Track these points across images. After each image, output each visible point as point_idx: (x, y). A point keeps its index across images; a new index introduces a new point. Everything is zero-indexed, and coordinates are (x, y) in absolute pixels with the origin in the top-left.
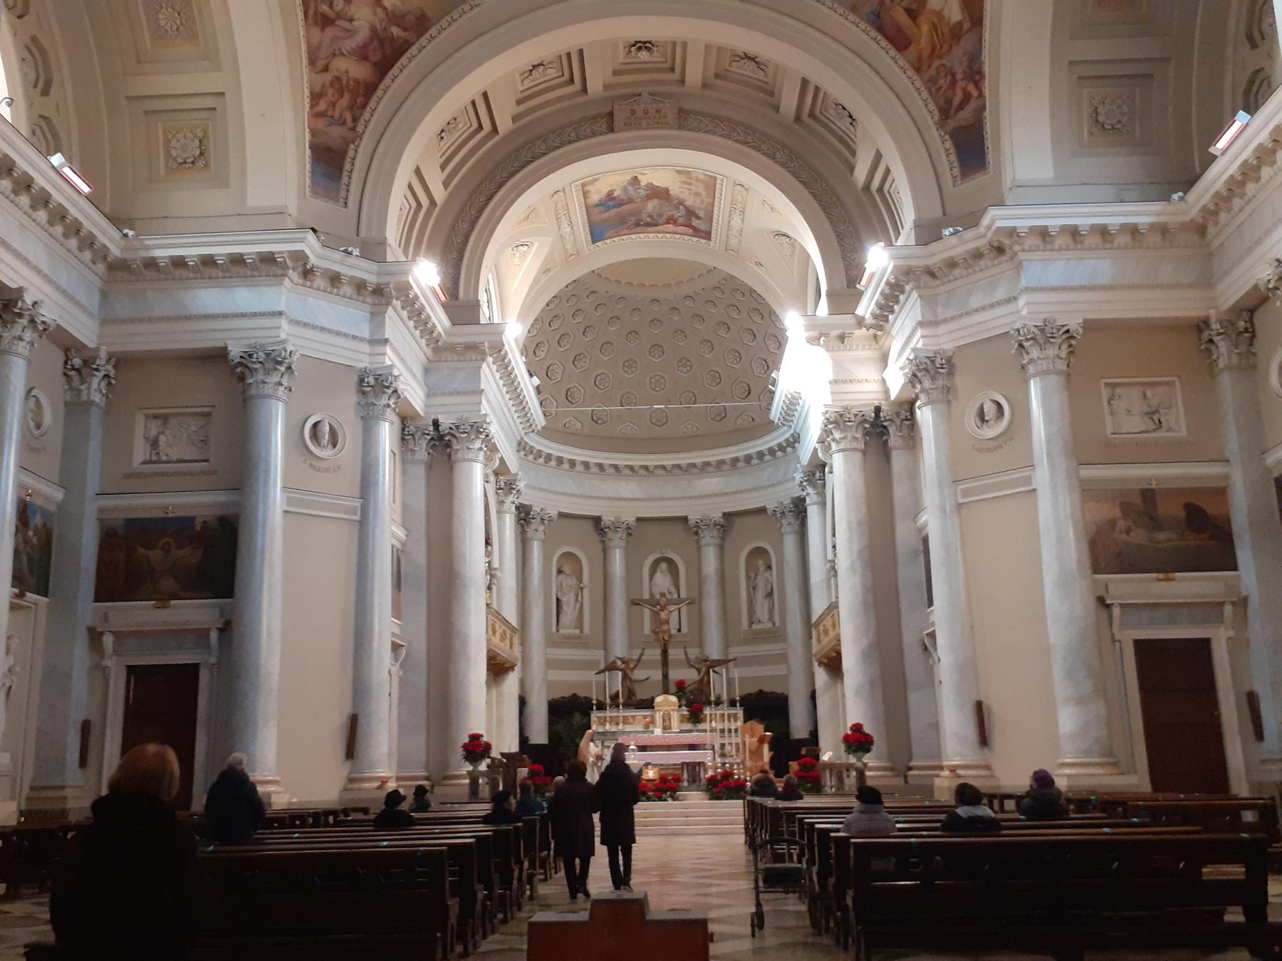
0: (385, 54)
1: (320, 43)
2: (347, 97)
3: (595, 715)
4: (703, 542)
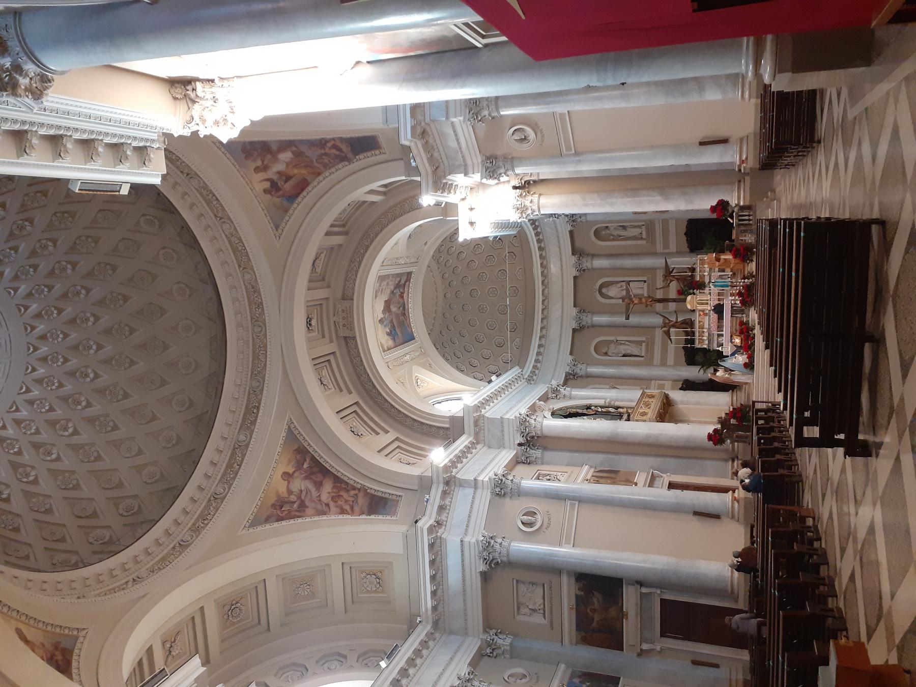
0: (318, 471)
2: (341, 493)
3: (697, 345)
4: (589, 266)
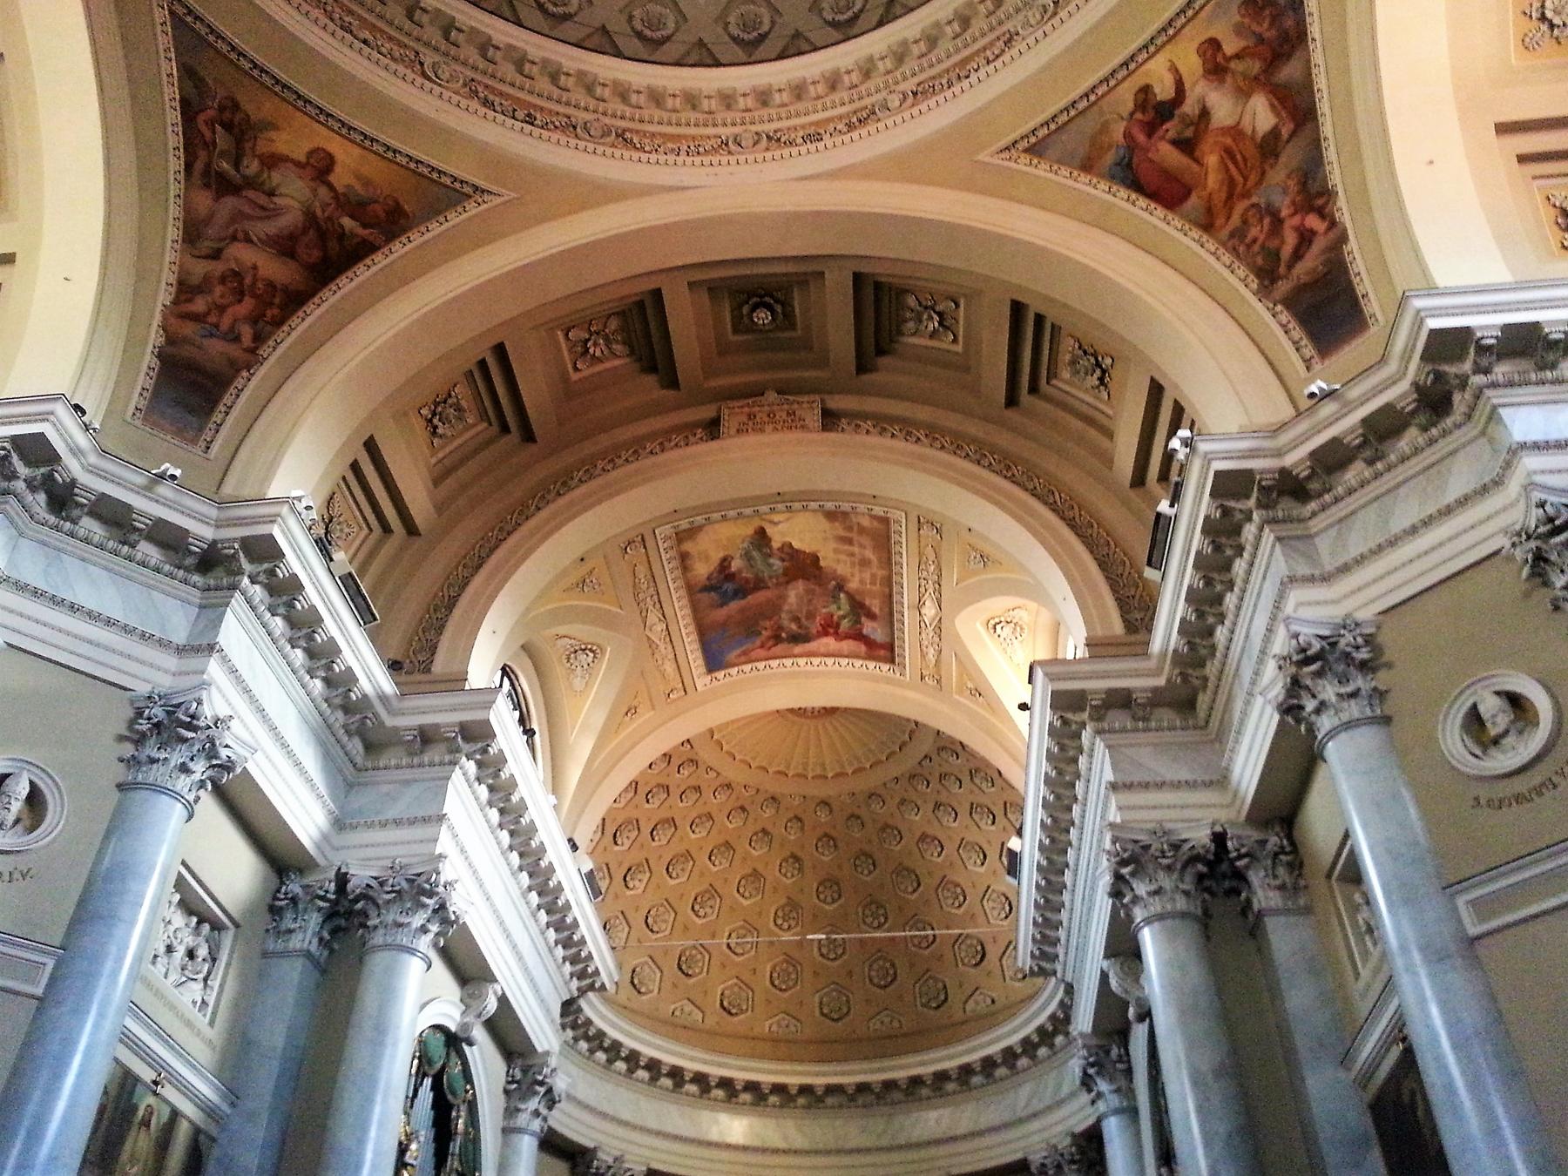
1: (211, 216)
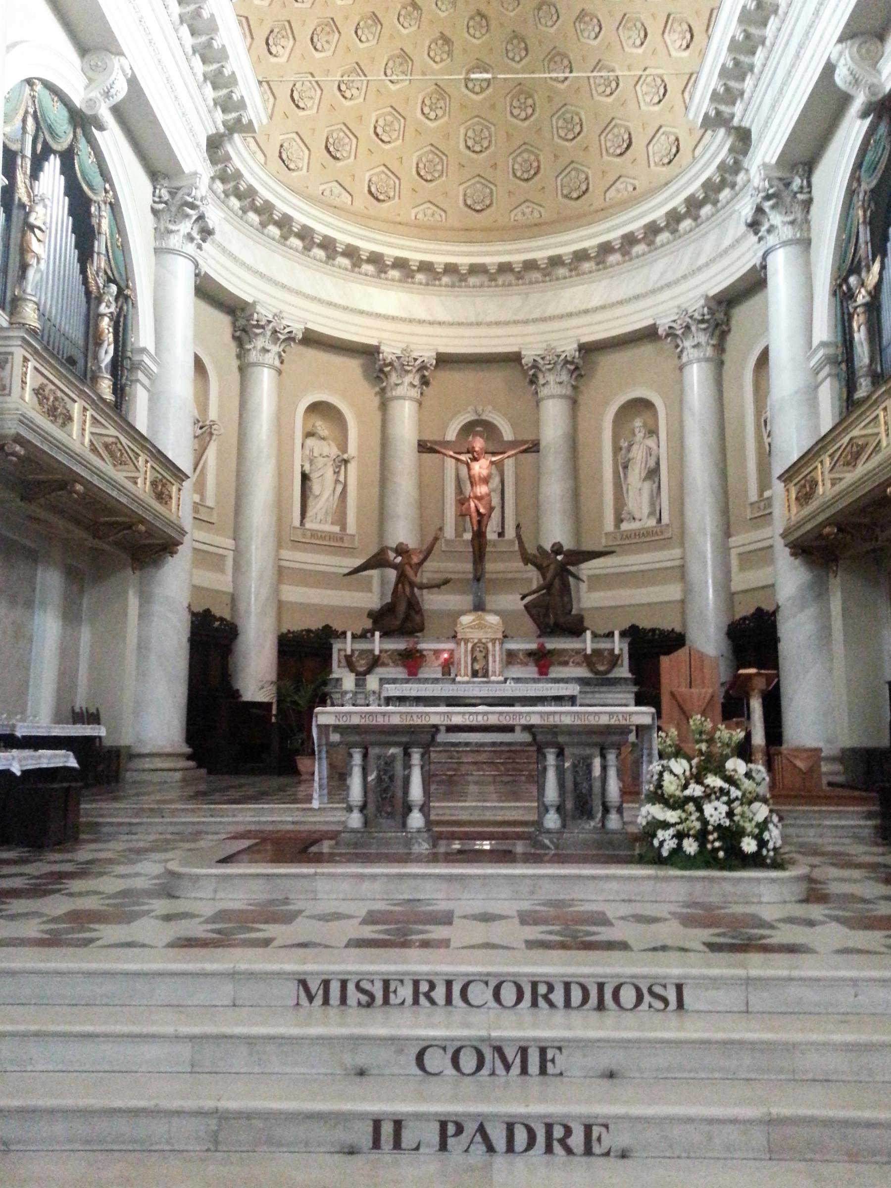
4: (544, 392)
